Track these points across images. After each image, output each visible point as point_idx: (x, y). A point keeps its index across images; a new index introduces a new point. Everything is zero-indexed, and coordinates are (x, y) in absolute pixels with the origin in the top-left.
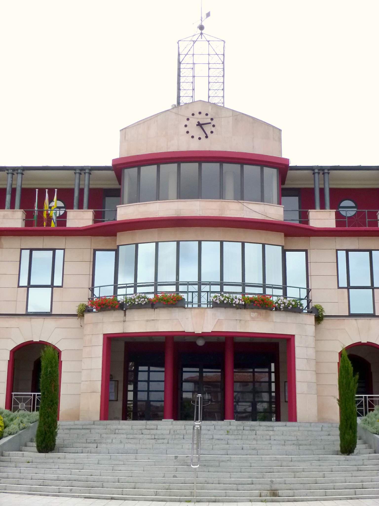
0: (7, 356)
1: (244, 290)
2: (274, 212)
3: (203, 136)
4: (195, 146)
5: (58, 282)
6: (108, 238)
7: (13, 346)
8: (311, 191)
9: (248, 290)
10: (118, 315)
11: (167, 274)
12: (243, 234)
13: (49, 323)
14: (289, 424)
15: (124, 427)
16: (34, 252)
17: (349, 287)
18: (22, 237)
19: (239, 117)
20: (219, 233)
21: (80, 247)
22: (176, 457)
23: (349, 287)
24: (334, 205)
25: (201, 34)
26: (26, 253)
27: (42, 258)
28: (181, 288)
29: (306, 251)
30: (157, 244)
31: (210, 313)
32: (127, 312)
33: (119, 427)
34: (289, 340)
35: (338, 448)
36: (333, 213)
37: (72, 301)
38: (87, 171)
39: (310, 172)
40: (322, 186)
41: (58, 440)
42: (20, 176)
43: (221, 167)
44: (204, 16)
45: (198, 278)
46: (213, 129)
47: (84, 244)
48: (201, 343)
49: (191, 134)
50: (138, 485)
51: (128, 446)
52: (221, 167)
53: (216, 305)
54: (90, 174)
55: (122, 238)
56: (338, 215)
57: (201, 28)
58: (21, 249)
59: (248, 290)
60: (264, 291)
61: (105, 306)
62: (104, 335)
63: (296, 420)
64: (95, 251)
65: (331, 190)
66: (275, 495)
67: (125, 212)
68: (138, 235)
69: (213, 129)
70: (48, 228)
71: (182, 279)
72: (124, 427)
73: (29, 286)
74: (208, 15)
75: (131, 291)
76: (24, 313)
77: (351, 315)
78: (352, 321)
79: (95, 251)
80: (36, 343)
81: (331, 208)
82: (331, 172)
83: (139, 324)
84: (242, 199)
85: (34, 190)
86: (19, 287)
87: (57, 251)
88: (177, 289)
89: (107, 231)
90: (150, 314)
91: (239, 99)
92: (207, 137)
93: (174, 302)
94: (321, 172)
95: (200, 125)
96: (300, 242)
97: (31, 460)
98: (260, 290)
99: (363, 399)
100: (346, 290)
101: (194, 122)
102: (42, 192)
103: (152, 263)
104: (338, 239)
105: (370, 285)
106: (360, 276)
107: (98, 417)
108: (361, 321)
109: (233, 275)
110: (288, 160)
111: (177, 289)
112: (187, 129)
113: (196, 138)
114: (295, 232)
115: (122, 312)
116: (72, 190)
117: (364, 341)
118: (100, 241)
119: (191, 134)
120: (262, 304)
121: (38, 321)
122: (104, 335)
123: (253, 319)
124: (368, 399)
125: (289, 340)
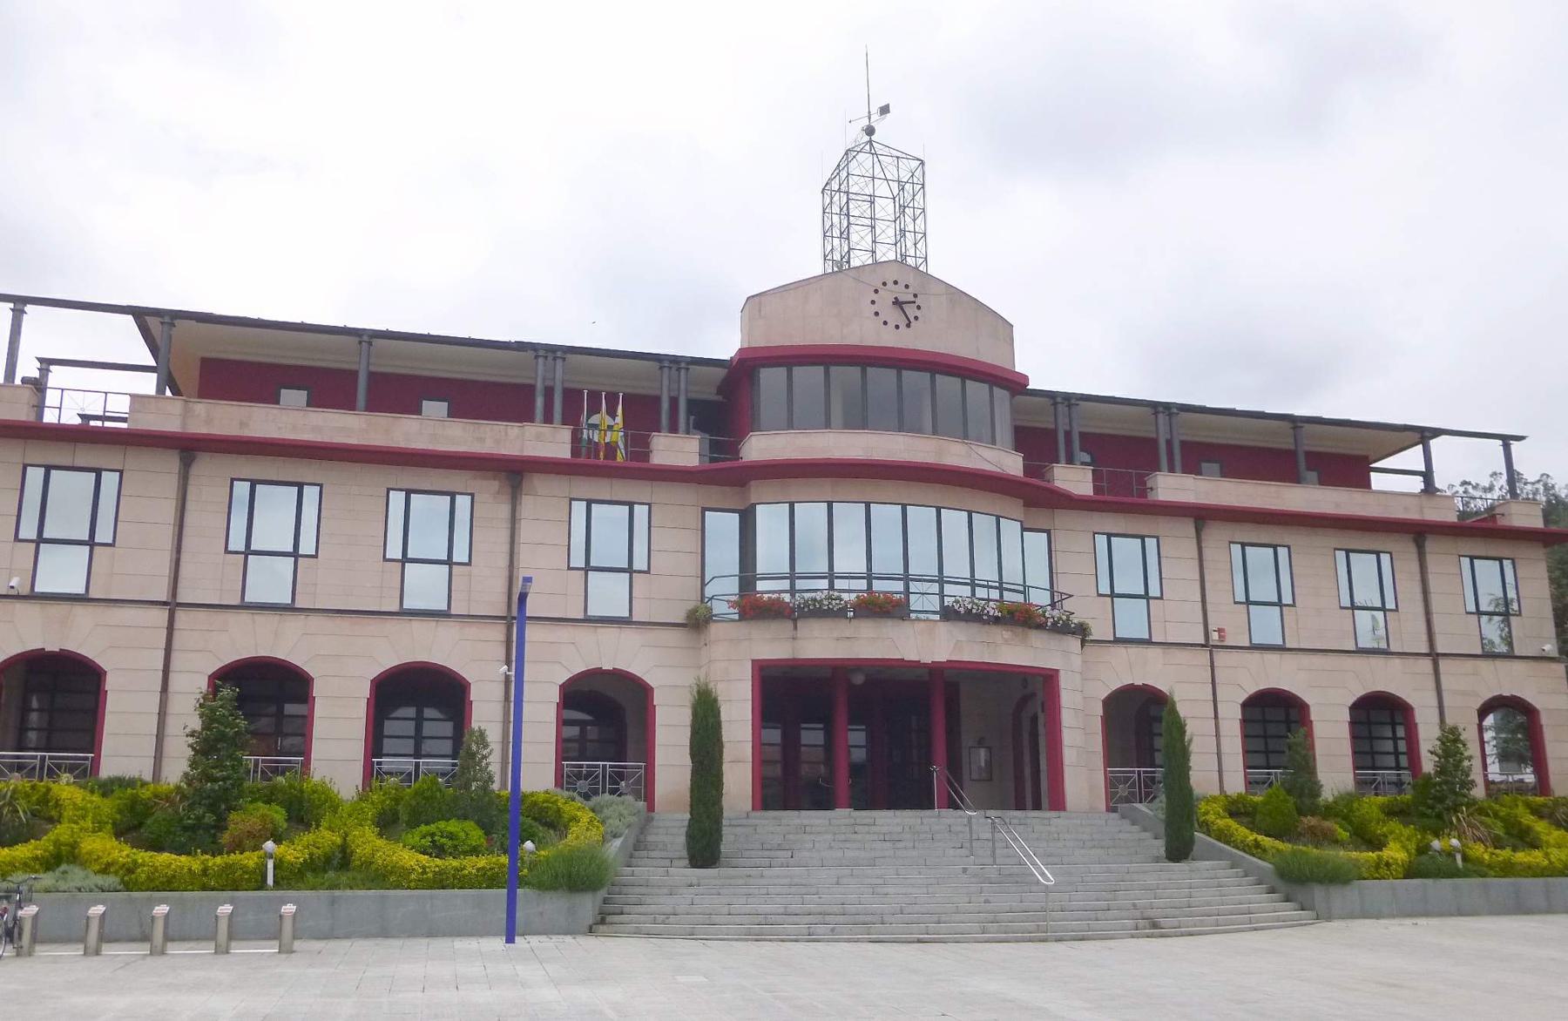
0: (366, 691)
1: (792, 585)
2: (1012, 464)
3: (902, 323)
4: (889, 338)
5: (103, 535)
6: (727, 489)
7: (564, 677)
8: (1050, 435)
9: (948, 589)
10: (782, 628)
11: (888, 558)
12: (869, 489)
13: (629, 637)
14: (1053, 814)
15: (817, 822)
16: (53, 473)
17: (588, 568)
18: (615, 481)
19: (956, 297)
20: (826, 487)
21: (678, 502)
22: (965, 870)
23: (588, 568)
24: (571, 417)
25: (870, 142)
26: (242, 489)
27: (609, 518)
28: (913, 587)
29: (321, 486)
30: (904, 507)
31: (945, 630)
32: (799, 624)
33: (806, 822)
34: (1049, 678)
35: (1162, 851)
36: (565, 434)
37: (667, 599)
38: (365, 338)
39: (656, 365)
40: (549, 383)
41: (725, 848)
42: (559, 363)
43: (864, 373)
44: (875, 109)
45: (912, 568)
46: (918, 313)
47: (687, 495)
48: (859, 679)
49: (882, 317)
50: (944, 918)
51: (849, 854)
52: (864, 373)
53: (948, 614)
54: (370, 344)
55: (757, 490)
56: (576, 439)
57: (870, 131)
58: (571, 499)
59: (948, 589)
60: (870, 585)
61: (753, 609)
62: (754, 662)
63: (1064, 809)
64: (232, 480)
65: (1082, 435)
66: (1155, 926)
67: (759, 447)
68: (796, 487)
69: (918, 313)
70: (610, 463)
71: (839, 568)
72: (817, 822)
73: (405, 559)
74: (885, 110)
75: (966, 591)
76: (581, 616)
77: (1118, 641)
78: (1120, 650)
79: (232, 480)
80: (608, 672)
81: (564, 423)
82: (568, 356)
83: (821, 643)
84: (966, 436)
85: (580, 392)
86: (569, 568)
87: (306, 489)
88: (907, 587)
89: (730, 478)
90: (1001, 634)
91: (949, 262)
92: (908, 326)
93: (881, 609)
94: (675, 367)
95: (897, 303)
96: (1040, 517)
97: (695, 881)
98: (863, 584)
99: (38, 762)
100: (97, 549)
101: (886, 297)
102: (594, 397)
103: (818, 541)
104: (1096, 516)
105: (253, 547)
106: (609, 548)
107: (750, 807)
108: (1134, 650)
109: (850, 559)
110: (1026, 378)
111: (907, 587)
112: (875, 308)
113: (891, 325)
114: (1034, 498)
115: (790, 624)
116: (657, 400)
117: (1138, 682)
118: (714, 494)
119: (882, 317)
120: (1020, 618)
121: (608, 634)
122: (754, 662)
123: (1006, 641)
124: (47, 762)
125: (1049, 678)
